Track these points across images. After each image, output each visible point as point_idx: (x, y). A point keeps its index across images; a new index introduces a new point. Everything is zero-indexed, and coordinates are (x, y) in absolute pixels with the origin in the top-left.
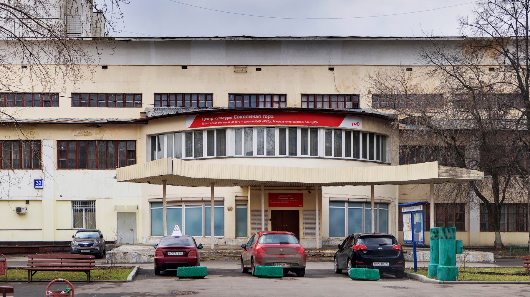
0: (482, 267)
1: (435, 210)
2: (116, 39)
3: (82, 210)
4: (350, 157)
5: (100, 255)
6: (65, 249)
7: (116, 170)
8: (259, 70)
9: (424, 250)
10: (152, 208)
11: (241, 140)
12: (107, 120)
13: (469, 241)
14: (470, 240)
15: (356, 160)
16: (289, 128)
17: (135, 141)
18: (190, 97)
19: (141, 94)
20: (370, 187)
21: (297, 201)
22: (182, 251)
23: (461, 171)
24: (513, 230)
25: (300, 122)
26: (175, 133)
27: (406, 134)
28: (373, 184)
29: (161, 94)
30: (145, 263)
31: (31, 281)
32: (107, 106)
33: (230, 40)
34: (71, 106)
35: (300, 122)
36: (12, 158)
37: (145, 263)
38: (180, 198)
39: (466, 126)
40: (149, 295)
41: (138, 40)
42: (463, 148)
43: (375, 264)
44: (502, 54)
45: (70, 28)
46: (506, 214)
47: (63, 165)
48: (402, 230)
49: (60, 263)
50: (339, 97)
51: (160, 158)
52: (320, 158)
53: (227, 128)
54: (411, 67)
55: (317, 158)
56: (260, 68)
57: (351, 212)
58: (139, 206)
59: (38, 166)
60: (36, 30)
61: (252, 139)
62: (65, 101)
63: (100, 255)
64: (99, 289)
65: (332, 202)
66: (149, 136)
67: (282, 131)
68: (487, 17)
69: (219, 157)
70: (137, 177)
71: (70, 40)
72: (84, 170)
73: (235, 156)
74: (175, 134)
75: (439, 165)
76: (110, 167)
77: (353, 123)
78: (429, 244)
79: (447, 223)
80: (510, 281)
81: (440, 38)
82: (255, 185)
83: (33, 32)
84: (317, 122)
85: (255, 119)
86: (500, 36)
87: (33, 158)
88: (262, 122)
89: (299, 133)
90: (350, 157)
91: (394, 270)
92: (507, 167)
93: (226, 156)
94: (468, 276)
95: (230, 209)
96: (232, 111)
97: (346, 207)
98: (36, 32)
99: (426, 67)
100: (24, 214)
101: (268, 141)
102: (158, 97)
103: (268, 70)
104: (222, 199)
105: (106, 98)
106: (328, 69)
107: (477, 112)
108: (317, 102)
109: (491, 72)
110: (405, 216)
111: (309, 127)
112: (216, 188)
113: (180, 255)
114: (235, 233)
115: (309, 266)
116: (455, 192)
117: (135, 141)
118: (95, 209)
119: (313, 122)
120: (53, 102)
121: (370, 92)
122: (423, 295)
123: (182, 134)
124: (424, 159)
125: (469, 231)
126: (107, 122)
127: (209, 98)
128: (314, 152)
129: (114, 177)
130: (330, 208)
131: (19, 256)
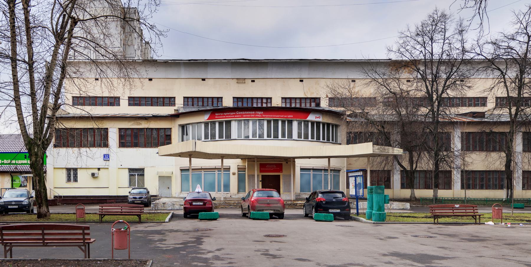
2: (158, 61)
3: (135, 175)
5: (499, 101)
6: (124, 201)
9: (363, 201)
15: (318, 141)
16: (274, 120)
17: (171, 129)
19: (175, 98)
20: (327, 159)
28: (329, 157)
29: (188, 98)
30: (177, 210)
31: (101, 222)
37: (177, 210)
40: (355, 265)
41: (172, 61)
43: (330, 211)
47: (123, 144)
49: (121, 210)
51: (187, 140)
52: (294, 140)
53: (232, 120)
55: (292, 140)
57: (314, 176)
59: (106, 145)
61: (248, 128)
62: (124, 102)
64: (146, 227)
65: (301, 169)
66: (180, 125)
67: (269, 122)
68: (455, 167)
69: (121, 198)
73: (237, 138)
75: (373, 144)
84: (292, 116)
85: (250, 114)
89: (280, 123)
94: (393, 219)
95: (234, 174)
97: (312, 172)
100: (97, 177)
102: (186, 100)
104: (229, 167)
105: (152, 100)
106: (299, 81)
107: (399, 109)
109: (408, 83)
111: (209, 121)
115: (287, 212)
116: (384, 162)
118: (144, 174)
124: (363, 141)
125: (454, 189)
128: (290, 136)
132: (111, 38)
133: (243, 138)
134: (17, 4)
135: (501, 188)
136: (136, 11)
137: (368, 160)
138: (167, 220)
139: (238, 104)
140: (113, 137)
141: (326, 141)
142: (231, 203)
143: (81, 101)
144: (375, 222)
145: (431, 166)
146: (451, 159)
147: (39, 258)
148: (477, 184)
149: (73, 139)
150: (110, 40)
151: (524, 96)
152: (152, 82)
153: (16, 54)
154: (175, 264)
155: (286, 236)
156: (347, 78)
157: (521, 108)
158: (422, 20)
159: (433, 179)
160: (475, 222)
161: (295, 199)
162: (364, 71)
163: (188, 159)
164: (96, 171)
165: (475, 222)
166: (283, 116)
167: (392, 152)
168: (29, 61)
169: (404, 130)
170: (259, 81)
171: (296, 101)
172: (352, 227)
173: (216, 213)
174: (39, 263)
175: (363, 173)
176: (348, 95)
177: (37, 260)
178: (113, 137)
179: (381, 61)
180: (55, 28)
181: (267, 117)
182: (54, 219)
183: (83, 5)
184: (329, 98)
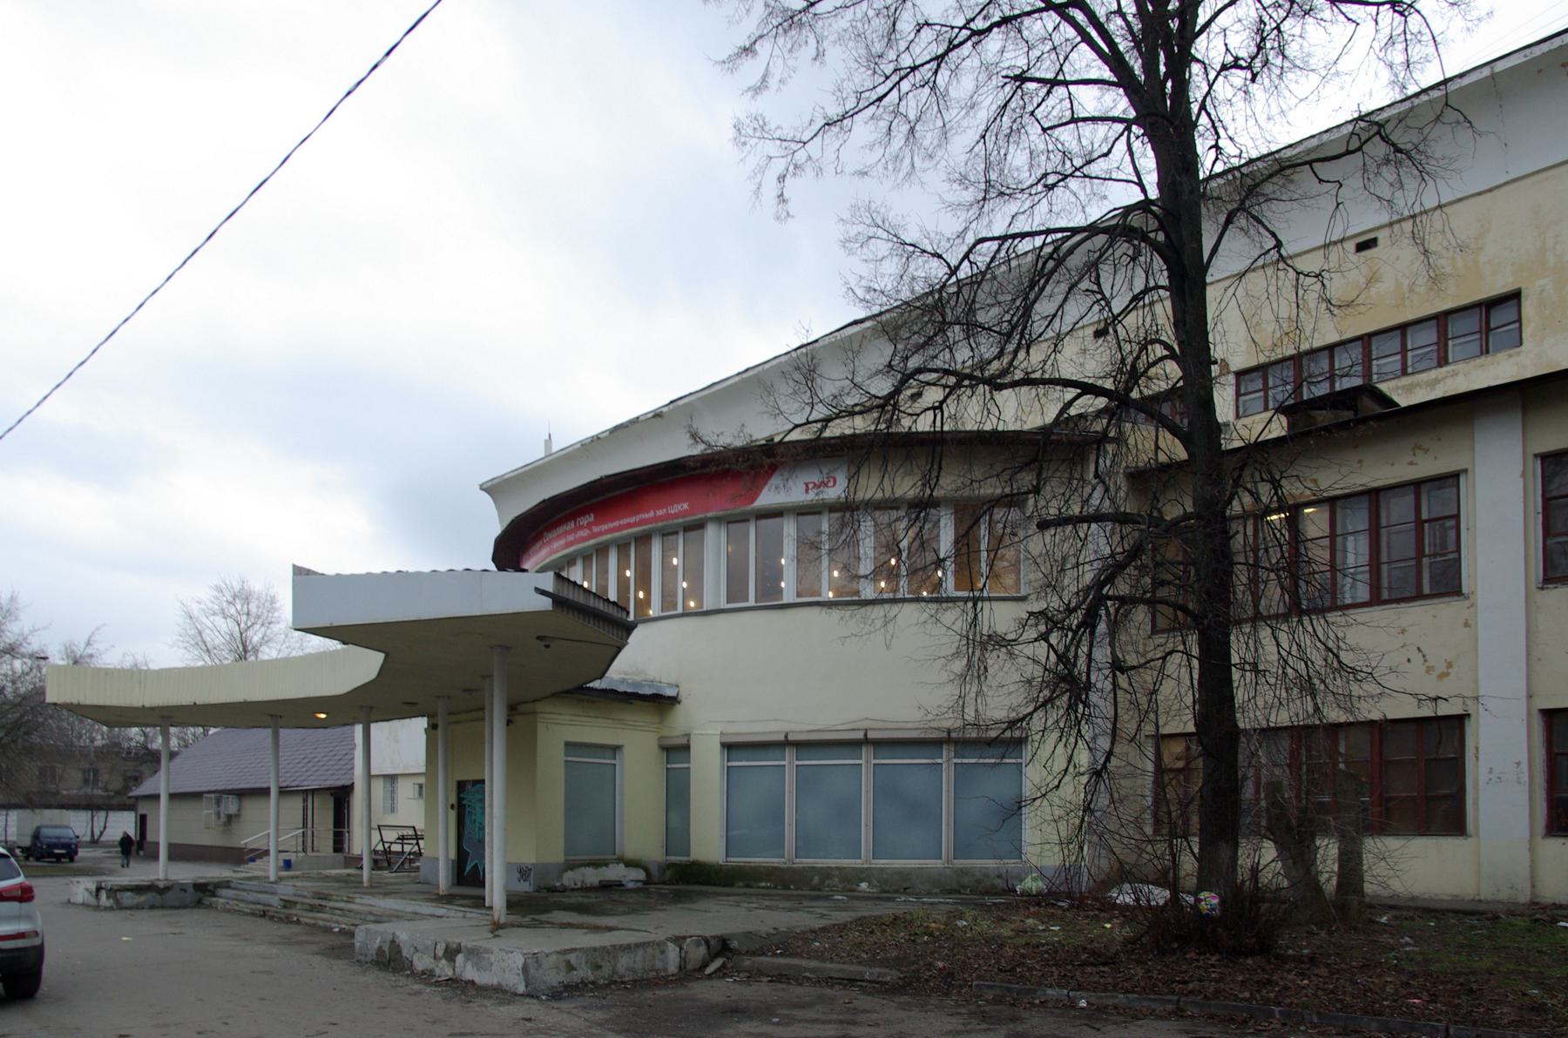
0: (727, 56)
2: (641, 418)
7: (495, 489)
10: (669, 766)
11: (437, 750)
14: (1399, 339)
18: (547, 589)
22: (862, 891)
23: (853, 1023)
25: (622, 522)
26: (729, 523)
27: (282, 916)
33: (827, 342)
34: (299, 564)
35: (622, 522)
36: (1384, 559)
38: (782, 732)
42: (653, 966)
43: (742, 904)
44: (1031, 247)
45: (1281, 274)
54: (1371, 236)
55: (1532, 834)
57: (806, 780)
58: (730, 50)
65: (730, 748)
70: (397, 48)
72: (512, 471)
73: (724, 605)
74: (730, 526)
75: (40, 692)
77: (807, 485)
78: (169, 809)
79: (1292, 885)
80: (555, 553)
81: (1388, 110)
82: (1023, 239)
84: (686, 506)
87: (1427, 551)
90: (747, 601)
93: (705, 609)
96: (1435, 534)
97: (789, 761)
98: (909, 73)
103: (1435, 458)
108: (1480, 332)
110: (1454, 548)
112: (400, 850)
113: (1229, 681)
119: (675, 509)
120: (783, 857)
123: (785, 523)
125: (1529, 714)
129: (93, 638)
130: (689, 762)
131: (1431, 899)
132: (863, 130)
133: (752, 602)
134: (1157, 431)
135: (1431, 589)
137: (305, 801)
142: (806, 970)
144: (869, 973)
147: (787, 585)
148: (824, 961)
149: (299, 906)
150: (1090, 495)
151: (978, 312)
152: (776, 181)
153: (815, 440)
154: (1057, 928)
157: (1255, 496)
159: (592, 542)
160: (372, 773)
163: (1399, 350)
165: (372, 773)
166: (652, 514)
168: (825, 438)
169: (866, 577)
170: (1360, 462)
171: (1404, 344)
172: (1477, 757)
173: (524, 916)
175: (1326, 832)
176: (224, 628)
177: (332, 928)
179: (1500, 67)
180: (936, 467)
181: (629, 525)
183: (921, 962)
184: (1240, 374)
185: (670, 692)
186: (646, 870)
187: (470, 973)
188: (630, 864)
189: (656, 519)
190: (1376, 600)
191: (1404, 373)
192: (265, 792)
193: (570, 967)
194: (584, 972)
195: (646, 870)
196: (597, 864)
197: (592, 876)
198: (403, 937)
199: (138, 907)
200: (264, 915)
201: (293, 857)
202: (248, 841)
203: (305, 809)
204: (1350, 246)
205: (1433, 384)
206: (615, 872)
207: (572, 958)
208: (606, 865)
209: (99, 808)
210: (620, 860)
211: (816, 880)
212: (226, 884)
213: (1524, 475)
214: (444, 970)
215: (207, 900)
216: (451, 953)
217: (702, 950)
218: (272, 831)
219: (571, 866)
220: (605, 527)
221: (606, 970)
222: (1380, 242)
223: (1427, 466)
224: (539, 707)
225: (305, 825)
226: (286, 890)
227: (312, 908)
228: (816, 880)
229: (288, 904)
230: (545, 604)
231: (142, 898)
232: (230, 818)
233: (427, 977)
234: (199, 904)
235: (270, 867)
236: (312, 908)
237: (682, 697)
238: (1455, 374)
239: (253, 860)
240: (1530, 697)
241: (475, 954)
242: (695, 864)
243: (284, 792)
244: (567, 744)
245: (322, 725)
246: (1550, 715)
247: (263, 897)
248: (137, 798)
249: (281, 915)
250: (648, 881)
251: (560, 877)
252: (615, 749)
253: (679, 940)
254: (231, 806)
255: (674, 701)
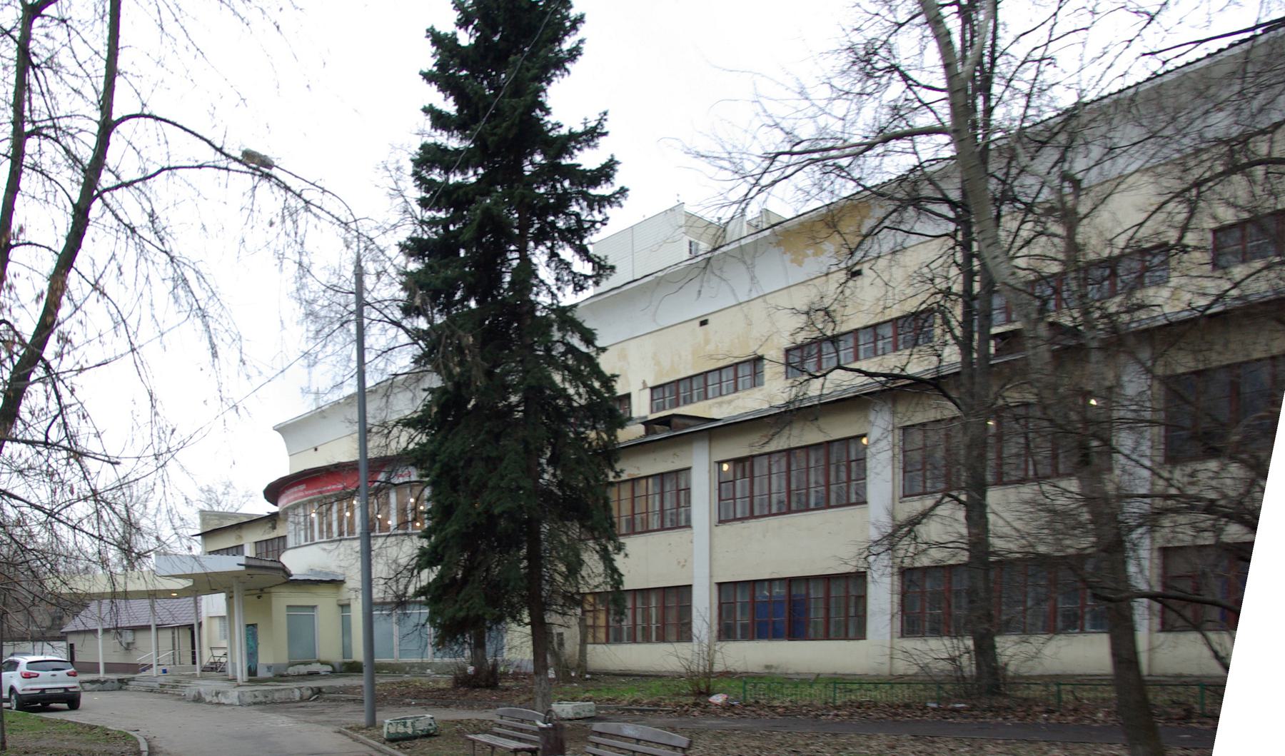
1: (817, 695)
4: (98, 672)
8: (704, 323)
12: (1166, 318)
13: (710, 447)
21: (469, 406)
24: (816, 592)
31: (679, 491)
32: (1249, 561)
39: (867, 138)
46: (812, 485)
48: (258, 545)
50: (724, 372)
56: (911, 644)
60: (902, 68)
63: (725, 467)
71: (75, 609)
75: (514, 619)
76: (1277, 409)
83: (550, 258)
86: (1213, 636)
88: (977, 278)
91: (1096, 725)
92: (1059, 692)
99: (873, 262)
101: (835, 683)
114: (362, 570)
115: (968, 26)
117: (242, 545)
121: (645, 387)
122: (1207, 112)
124: (1277, 409)
125: (710, 585)
126: (55, 643)
127: (672, 602)
136: (1059, 176)
137: (173, 633)
138: (98, 730)
139: (1243, 280)
140: (703, 607)
141: (325, 540)
143: (482, 727)
145: (555, 339)
146: (26, 528)
155: (281, 270)
156: (734, 303)
158: (614, 275)
161: (578, 25)
162: (874, 189)
164: (1096, 17)
167: (1248, 356)
174: (1185, 249)
178: (703, 607)
182: (1113, 52)
184: (653, 389)
185: (341, 578)
186: (332, 666)
187: (223, 700)
188: (323, 663)
189: (333, 490)
190: (662, 528)
191: (721, 395)
192: (147, 628)
193: (256, 697)
194: (261, 698)
195: (332, 666)
196: (305, 664)
197: (303, 669)
198: (202, 690)
199: (93, 690)
200: (152, 691)
201: (167, 668)
202: (140, 659)
203: (173, 638)
204: (697, 322)
205: (739, 403)
206: (315, 667)
207: (256, 693)
208: (310, 664)
209: (38, 640)
210: (318, 661)
211: (408, 669)
212: (133, 679)
213: (710, 471)
214: (215, 700)
215: (124, 687)
216: (217, 694)
217: (309, 692)
218: (154, 652)
219: (292, 665)
220: (310, 492)
221: (270, 698)
222: (710, 322)
223: (677, 465)
224: (273, 590)
225: (174, 649)
226: (162, 680)
227: (173, 687)
228: (408, 669)
229: (162, 685)
230: (242, 568)
231: (94, 686)
232: (128, 644)
233: (210, 703)
234: (120, 689)
235: (155, 671)
236: (173, 687)
237: (347, 580)
238: (738, 398)
239: (144, 670)
240: (711, 576)
241: (224, 693)
242: (354, 662)
243: (159, 627)
244: (288, 606)
245: (174, 598)
246: (720, 585)
247: (151, 684)
248: (67, 633)
249: (161, 690)
250: (334, 672)
251: (286, 670)
252: (314, 607)
253: (299, 688)
254: (128, 637)
255: (342, 582)
